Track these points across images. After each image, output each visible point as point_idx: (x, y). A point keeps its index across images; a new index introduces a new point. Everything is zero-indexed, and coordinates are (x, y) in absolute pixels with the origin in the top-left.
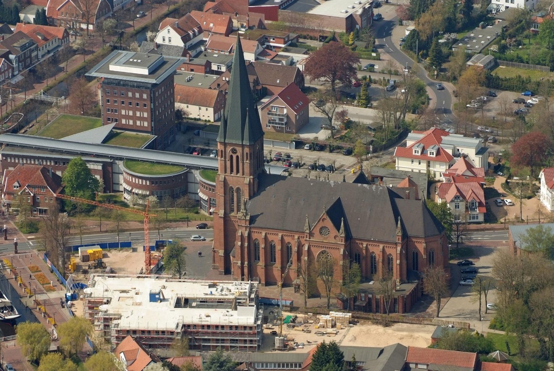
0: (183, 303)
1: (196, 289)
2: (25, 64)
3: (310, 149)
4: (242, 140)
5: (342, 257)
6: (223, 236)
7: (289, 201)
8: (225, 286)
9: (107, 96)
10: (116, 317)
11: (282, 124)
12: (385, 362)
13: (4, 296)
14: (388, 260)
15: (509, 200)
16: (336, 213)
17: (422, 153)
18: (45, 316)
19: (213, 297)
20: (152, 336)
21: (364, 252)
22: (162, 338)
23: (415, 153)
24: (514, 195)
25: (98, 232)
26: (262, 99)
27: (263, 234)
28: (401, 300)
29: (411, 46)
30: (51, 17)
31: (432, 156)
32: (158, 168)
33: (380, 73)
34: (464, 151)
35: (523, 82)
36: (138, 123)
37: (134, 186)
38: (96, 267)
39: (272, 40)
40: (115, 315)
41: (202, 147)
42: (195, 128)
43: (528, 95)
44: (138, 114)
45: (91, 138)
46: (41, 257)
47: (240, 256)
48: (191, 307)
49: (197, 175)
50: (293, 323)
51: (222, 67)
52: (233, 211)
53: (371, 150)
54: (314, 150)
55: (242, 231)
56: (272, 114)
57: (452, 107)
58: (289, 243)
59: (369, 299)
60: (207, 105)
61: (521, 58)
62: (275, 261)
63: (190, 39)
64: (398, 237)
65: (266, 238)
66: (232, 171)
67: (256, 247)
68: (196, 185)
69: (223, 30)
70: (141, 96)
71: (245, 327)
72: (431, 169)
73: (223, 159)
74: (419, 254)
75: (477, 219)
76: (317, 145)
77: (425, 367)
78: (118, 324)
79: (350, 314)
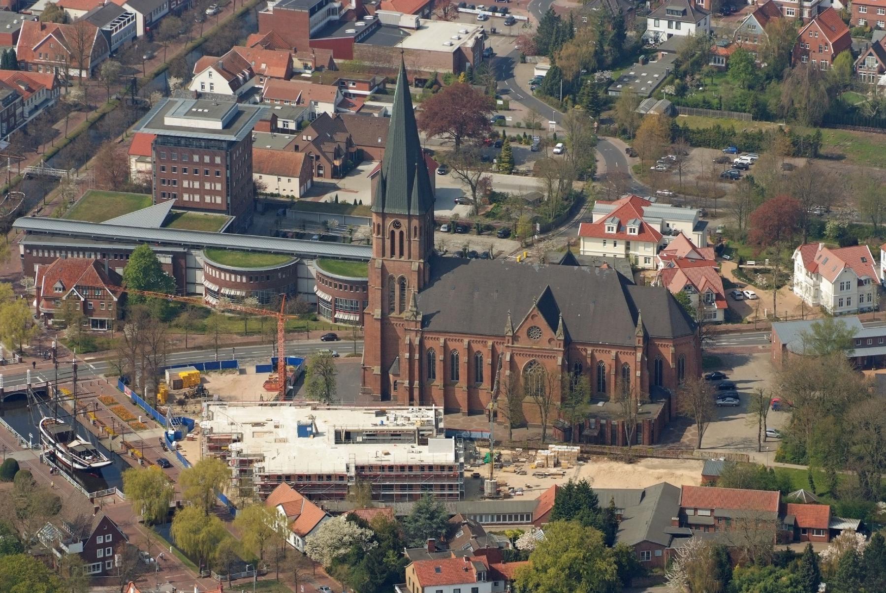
0: (345, 437)
1: (361, 419)
2: (8, 124)
3: (449, 231)
4: (409, 209)
5: (560, 368)
7: (476, 294)
8: (399, 413)
9: (162, 161)
10: (258, 458)
12: (655, 508)
13: (78, 437)
14: (623, 371)
15: (751, 292)
16: (549, 307)
17: (618, 230)
18: (142, 463)
20: (314, 482)
21: (589, 361)
22: (328, 485)
24: (756, 285)
25: (182, 350)
26: (358, 165)
27: (442, 341)
29: (552, 89)
30: (23, 61)
31: (632, 234)
32: (255, 258)
33: (514, 127)
34: (675, 226)
35: (724, 134)
36: (208, 199)
37: (222, 284)
38: (194, 396)
39: (351, 85)
40: (254, 455)
41: (298, 231)
42: (277, 206)
43: (732, 152)
44: (207, 186)
45: (146, 220)
46: (114, 382)
47: (407, 372)
49: (313, 268)
50: (498, 463)
51: (290, 124)
52: (393, 310)
53: (538, 229)
54: (455, 232)
55: (409, 338)
57: (630, 171)
58: (479, 352)
59: (602, 425)
60: (289, 174)
61: (708, 103)
62: (458, 379)
63: (240, 86)
65: (445, 346)
66: (393, 253)
67: (431, 360)
68: (310, 281)
69: (282, 72)
70: (212, 160)
71: (442, 467)
72: (631, 252)
73: (380, 236)
74: (664, 365)
75: (715, 317)
76: (457, 225)
77: (708, 513)
78: (263, 468)
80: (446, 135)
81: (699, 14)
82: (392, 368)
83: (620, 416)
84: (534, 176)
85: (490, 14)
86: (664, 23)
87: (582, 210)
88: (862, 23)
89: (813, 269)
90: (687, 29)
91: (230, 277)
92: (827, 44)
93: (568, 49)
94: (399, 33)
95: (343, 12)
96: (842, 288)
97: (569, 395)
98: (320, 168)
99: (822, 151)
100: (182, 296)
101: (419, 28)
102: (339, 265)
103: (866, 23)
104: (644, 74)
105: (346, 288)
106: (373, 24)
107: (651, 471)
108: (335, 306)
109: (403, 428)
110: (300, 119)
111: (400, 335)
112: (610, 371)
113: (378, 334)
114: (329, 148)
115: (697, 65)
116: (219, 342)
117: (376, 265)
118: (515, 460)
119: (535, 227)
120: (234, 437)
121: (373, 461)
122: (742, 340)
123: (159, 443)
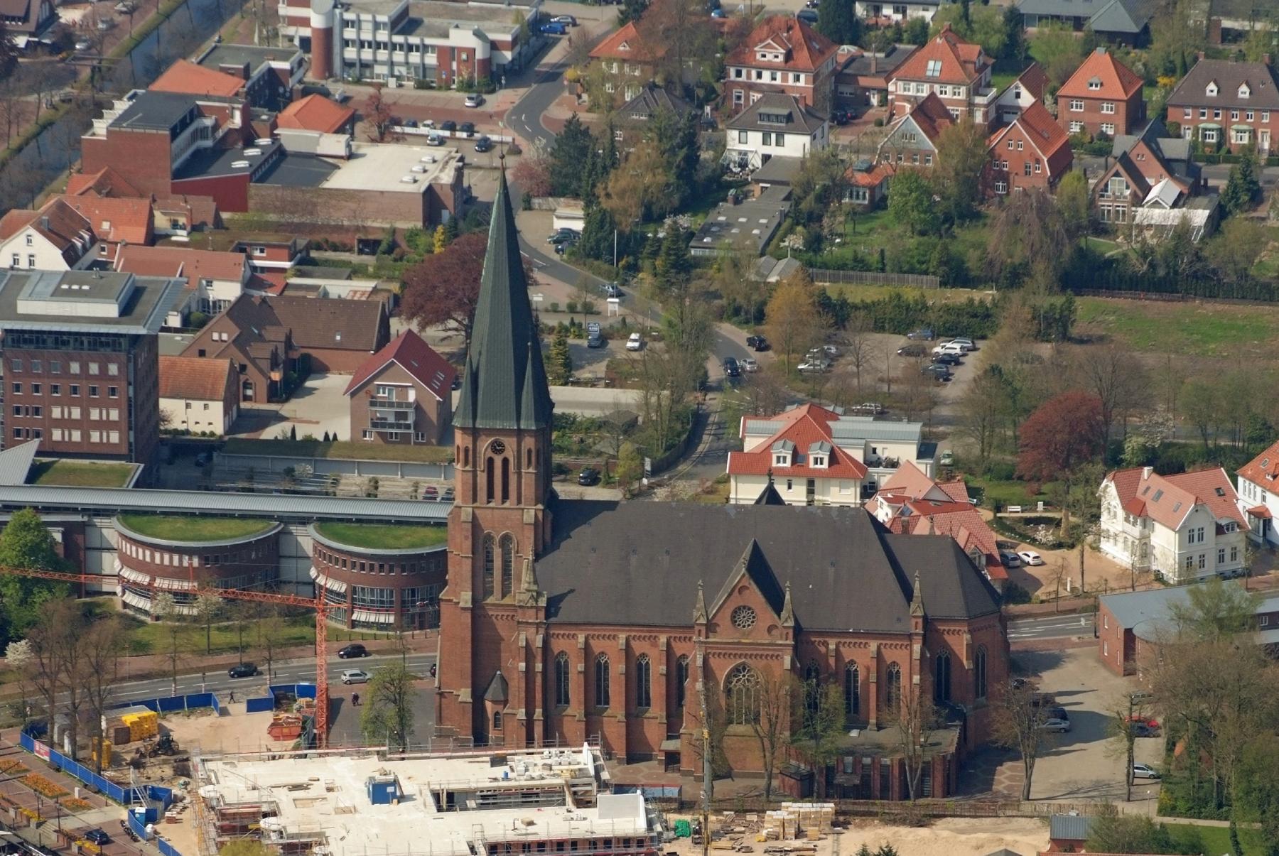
1: (472, 772)
6: (470, 655)
7: (634, 559)
9: (15, 376)
11: (408, 427)
14: (888, 676)
15: (1033, 554)
17: (794, 462)
19: (512, 783)
21: (832, 661)
23: (778, 461)
26: (305, 380)
27: (581, 639)
28: (939, 767)
31: (819, 466)
32: (209, 527)
34: (887, 451)
35: (908, 308)
37: (154, 571)
39: (257, 253)
44: (95, 414)
47: (523, 695)
48: (465, 809)
49: (307, 539)
53: (648, 467)
56: (382, 404)
58: (644, 655)
60: (204, 395)
61: (862, 261)
62: (607, 703)
64: (913, 621)
66: (490, 496)
68: (300, 561)
69: (139, 234)
70: (104, 370)
71: (627, 841)
73: (468, 468)
79: (832, 805)
80: (452, 324)
81: (813, 121)
82: (491, 690)
83: (894, 751)
84: (607, 386)
85: (447, 133)
86: (755, 138)
87: (705, 437)
88: (1075, 128)
89: (1136, 509)
90: (795, 146)
91: (171, 560)
92: (1038, 161)
93: (617, 182)
94: (324, 165)
95: (220, 133)
96: (1191, 539)
97: (808, 714)
98: (247, 385)
99: (1074, 331)
100: (79, 597)
101: (351, 156)
102: (352, 530)
103: (1082, 128)
104: (742, 220)
105: (372, 568)
106: (274, 152)
107: (963, 837)
108: (353, 599)
109: (543, 782)
110: (186, 311)
111: (503, 634)
112: (867, 678)
113: (468, 634)
114: (262, 352)
115: (825, 197)
116: (180, 666)
117: (463, 518)
118: (726, 831)
119: (643, 465)
120: (265, 809)
121: (511, 837)
122: (1040, 629)
123: (121, 830)
